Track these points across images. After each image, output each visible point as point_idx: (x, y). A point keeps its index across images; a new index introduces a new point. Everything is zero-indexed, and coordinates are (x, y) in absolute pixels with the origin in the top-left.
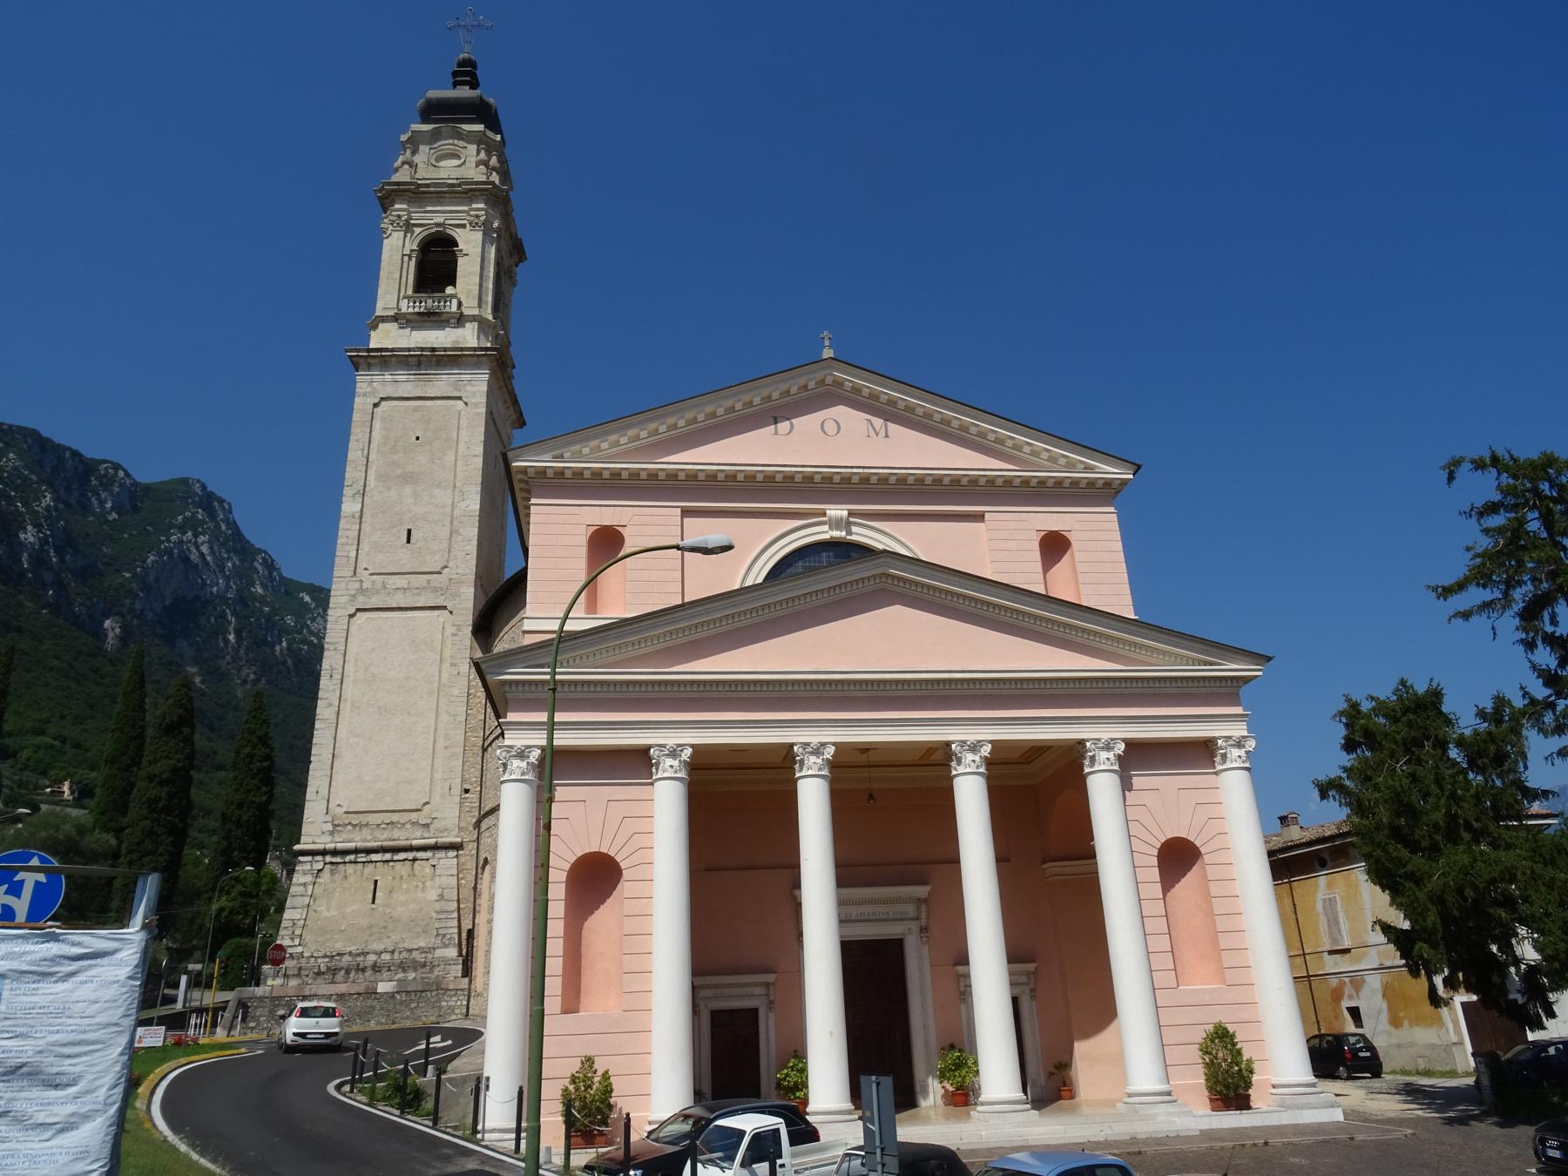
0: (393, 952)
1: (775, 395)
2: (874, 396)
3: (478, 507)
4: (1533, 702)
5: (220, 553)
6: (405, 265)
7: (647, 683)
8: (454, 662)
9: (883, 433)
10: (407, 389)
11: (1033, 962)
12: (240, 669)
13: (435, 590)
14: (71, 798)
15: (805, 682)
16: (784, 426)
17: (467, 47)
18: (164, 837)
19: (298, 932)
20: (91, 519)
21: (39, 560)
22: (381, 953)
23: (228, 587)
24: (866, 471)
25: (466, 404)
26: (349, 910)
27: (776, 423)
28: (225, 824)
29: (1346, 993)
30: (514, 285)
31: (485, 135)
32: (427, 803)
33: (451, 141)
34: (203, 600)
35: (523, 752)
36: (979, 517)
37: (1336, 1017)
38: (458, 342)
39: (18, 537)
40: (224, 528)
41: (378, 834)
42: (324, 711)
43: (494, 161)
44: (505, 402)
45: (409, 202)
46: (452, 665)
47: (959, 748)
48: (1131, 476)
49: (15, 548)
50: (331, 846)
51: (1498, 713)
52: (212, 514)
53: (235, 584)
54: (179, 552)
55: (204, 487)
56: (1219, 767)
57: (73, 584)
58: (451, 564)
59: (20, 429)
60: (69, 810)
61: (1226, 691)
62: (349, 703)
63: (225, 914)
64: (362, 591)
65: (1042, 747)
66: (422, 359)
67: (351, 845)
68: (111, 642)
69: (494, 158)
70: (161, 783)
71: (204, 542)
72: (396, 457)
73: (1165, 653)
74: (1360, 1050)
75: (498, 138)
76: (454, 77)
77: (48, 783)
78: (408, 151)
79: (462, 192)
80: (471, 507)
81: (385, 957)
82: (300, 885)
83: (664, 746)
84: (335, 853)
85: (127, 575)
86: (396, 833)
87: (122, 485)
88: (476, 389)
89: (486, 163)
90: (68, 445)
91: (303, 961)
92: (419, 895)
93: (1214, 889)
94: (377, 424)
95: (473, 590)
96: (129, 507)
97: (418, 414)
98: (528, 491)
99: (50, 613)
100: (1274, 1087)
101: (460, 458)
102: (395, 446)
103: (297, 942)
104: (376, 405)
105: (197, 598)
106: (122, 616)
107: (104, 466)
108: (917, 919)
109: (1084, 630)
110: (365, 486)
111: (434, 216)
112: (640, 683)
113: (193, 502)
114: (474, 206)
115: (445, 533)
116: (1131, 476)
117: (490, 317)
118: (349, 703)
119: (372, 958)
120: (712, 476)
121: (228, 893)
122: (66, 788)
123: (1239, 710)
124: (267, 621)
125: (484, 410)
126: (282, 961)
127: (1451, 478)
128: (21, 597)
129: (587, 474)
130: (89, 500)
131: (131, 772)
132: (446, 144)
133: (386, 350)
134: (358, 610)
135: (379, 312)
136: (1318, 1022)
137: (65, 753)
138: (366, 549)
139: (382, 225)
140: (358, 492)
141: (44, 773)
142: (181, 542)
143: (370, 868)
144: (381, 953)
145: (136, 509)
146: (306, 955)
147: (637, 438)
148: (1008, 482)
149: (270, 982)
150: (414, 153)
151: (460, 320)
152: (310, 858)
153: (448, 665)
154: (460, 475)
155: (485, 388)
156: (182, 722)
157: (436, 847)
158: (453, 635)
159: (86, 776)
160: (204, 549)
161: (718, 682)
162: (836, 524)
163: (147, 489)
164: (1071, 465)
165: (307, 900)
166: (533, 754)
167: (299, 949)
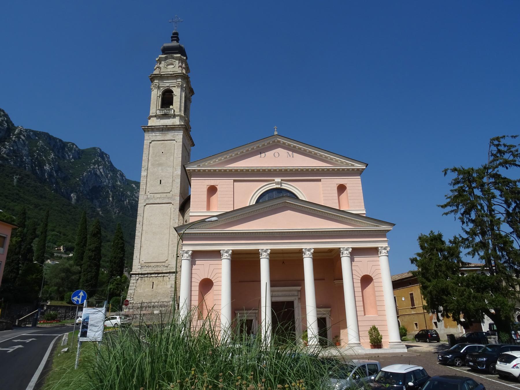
0: (158, 302)
1: (260, 146)
2: (289, 145)
3: (180, 173)
4: (463, 239)
5: (106, 171)
6: (158, 99)
7: (220, 233)
8: (174, 219)
9: (292, 156)
10: (159, 138)
11: (330, 308)
12: (114, 209)
13: (168, 198)
14: (63, 251)
15: (262, 232)
16: (263, 155)
17: (175, 28)
18: (94, 267)
19: (132, 296)
20: (66, 161)
21: (50, 175)
22: (155, 302)
23: (109, 183)
24: (286, 168)
25: (176, 142)
26: (146, 290)
27: (261, 154)
28: (111, 263)
29: (434, 318)
30: (191, 102)
31: (181, 57)
32: (167, 260)
33: (171, 60)
34: (101, 187)
35: (187, 252)
36: (320, 180)
37: (431, 325)
38: (174, 123)
39: (44, 168)
40: (107, 163)
41: (153, 269)
42: (138, 234)
43: (184, 66)
44: (188, 139)
45: (159, 80)
46: (173, 220)
47: (305, 250)
48: (365, 167)
49: (43, 171)
50: (140, 272)
51: (455, 241)
52: (103, 159)
53: (111, 181)
54: (93, 171)
55: (100, 150)
56: (379, 255)
57: (61, 183)
58: (172, 190)
59: (43, 133)
60: (63, 255)
61: (382, 234)
62: (145, 231)
63: (112, 290)
64: (148, 198)
65: (332, 249)
66: (164, 128)
67: (146, 272)
68: (73, 201)
69: (184, 64)
70: (92, 251)
71: (101, 168)
72: (156, 158)
73: (365, 223)
74: (433, 334)
75: (185, 58)
76: (172, 38)
77: (56, 247)
78: (158, 64)
79: (174, 76)
80: (178, 173)
81: (156, 304)
82: (132, 283)
83: (224, 250)
84: (142, 274)
85: (78, 179)
86: (159, 269)
87: (75, 150)
88: (179, 137)
89: (181, 67)
90: (58, 137)
91: (134, 304)
92: (165, 286)
93: (376, 289)
94: (151, 148)
95: (179, 198)
96: (77, 157)
97: (163, 145)
98: (191, 175)
99: (54, 192)
100: (390, 343)
101: (175, 158)
102: (156, 155)
103: (132, 299)
104: (150, 143)
105: (100, 186)
106: (76, 192)
107: (69, 144)
108: (298, 296)
109: (341, 217)
110: (148, 167)
111: (167, 84)
112: (218, 233)
113: (97, 155)
114: (178, 80)
115: (171, 181)
116: (365, 167)
117: (183, 115)
118: (145, 231)
119: (153, 304)
120: (242, 170)
121: (113, 284)
122: (62, 248)
123: (386, 239)
124: (122, 194)
125: (182, 143)
126: (128, 304)
127: (445, 174)
128: (46, 187)
129: (207, 171)
130: (65, 155)
131: (84, 248)
132: (169, 61)
133: (153, 126)
134: (147, 204)
135: (151, 114)
136: (426, 326)
137: (61, 237)
138: (149, 186)
139: (151, 87)
140: (146, 169)
141: (55, 243)
142: (94, 168)
143: (151, 278)
144: (155, 302)
145: (79, 158)
146: (134, 303)
147: (221, 160)
148: (328, 170)
149: (125, 310)
150: (160, 63)
151: (174, 116)
152: (135, 276)
153: (172, 220)
154: (175, 164)
155: (182, 137)
156: (97, 234)
157: (170, 273)
158: (174, 211)
159: (68, 244)
160: (101, 170)
161: (239, 233)
162: (277, 183)
163: (83, 151)
164: (347, 164)
165: (134, 287)
166: (190, 252)
167: (133, 301)
